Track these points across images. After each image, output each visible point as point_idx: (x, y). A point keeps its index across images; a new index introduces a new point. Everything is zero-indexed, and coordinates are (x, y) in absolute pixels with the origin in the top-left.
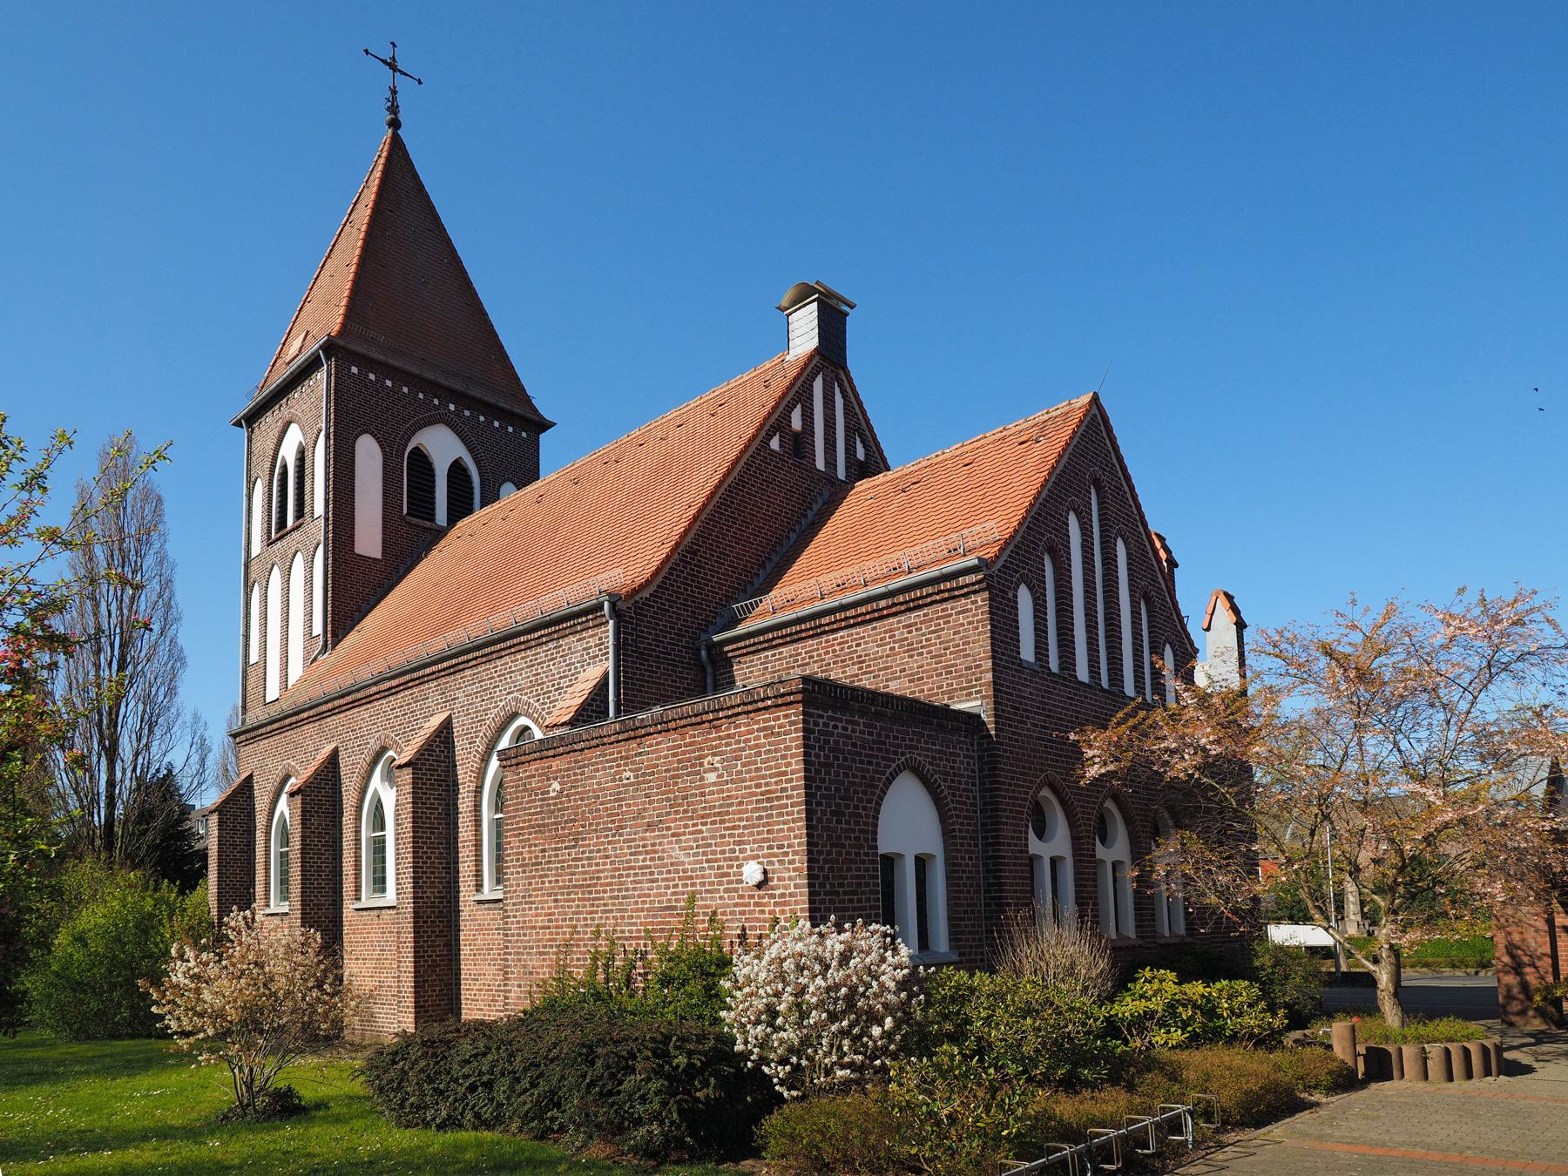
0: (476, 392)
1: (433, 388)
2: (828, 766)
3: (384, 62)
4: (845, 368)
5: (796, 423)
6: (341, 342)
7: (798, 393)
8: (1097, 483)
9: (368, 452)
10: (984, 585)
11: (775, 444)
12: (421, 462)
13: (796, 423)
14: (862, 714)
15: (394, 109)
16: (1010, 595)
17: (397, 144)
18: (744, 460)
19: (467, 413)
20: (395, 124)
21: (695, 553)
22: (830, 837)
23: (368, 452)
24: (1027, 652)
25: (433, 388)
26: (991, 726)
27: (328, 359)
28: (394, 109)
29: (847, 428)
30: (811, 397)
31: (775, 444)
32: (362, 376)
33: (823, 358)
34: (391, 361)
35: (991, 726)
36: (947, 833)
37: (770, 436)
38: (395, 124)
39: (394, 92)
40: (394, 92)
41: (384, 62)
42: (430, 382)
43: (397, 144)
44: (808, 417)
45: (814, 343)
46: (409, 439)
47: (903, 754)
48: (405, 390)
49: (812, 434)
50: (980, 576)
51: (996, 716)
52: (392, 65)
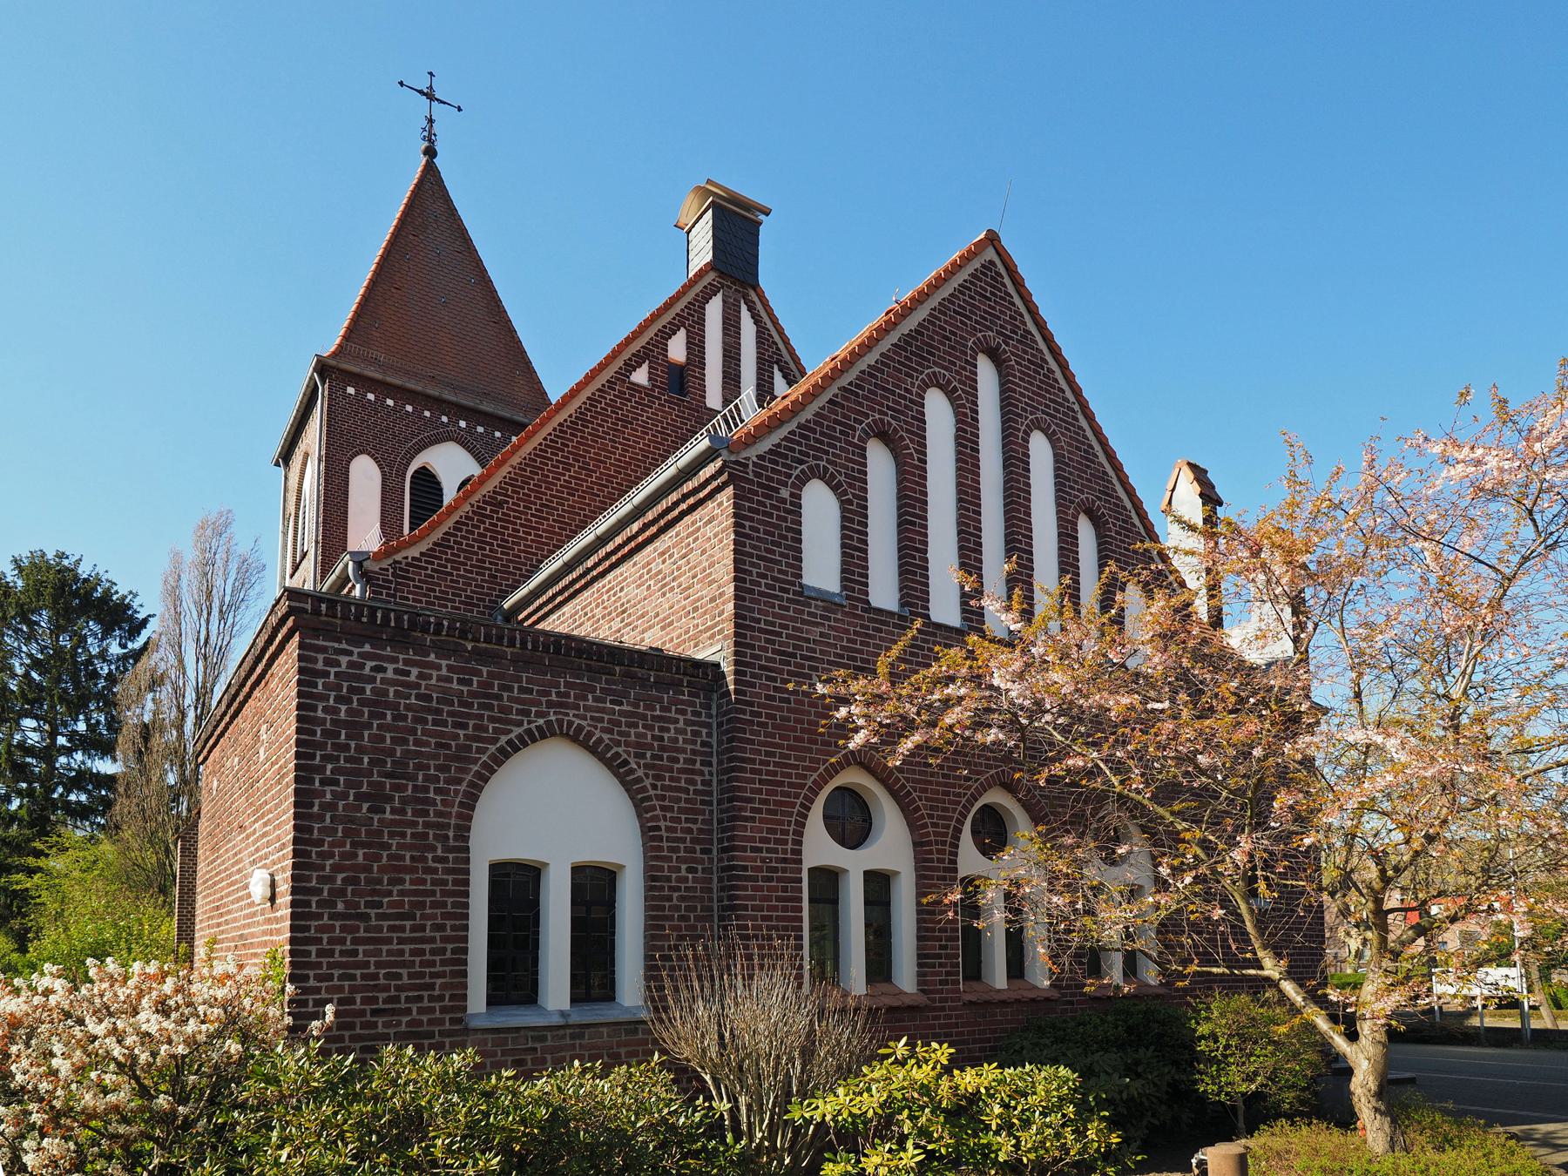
0: (487, 407)
1: (438, 404)
2: (355, 729)
3: (421, 92)
4: (755, 286)
5: (677, 349)
6: (333, 363)
7: (684, 313)
8: (994, 355)
9: (365, 475)
10: (724, 477)
11: (641, 376)
12: (427, 482)
13: (677, 349)
14: (443, 651)
15: (430, 138)
16: (785, 493)
17: (431, 171)
18: (587, 392)
19: (480, 429)
20: (430, 152)
21: (500, 504)
22: (347, 833)
23: (365, 475)
24: (821, 569)
25: (438, 404)
26: (730, 678)
27: (323, 383)
28: (430, 138)
29: (760, 360)
30: (701, 322)
31: (641, 376)
32: (359, 398)
33: (722, 274)
34: (389, 379)
35: (730, 678)
36: (649, 833)
37: (631, 366)
38: (430, 152)
39: (431, 121)
40: (431, 121)
41: (421, 92)
42: (486, 414)
43: (431, 171)
44: (696, 346)
45: (708, 257)
46: (413, 457)
47: (539, 715)
48: (409, 408)
49: (702, 366)
50: (719, 463)
51: (736, 663)
52: (429, 95)
